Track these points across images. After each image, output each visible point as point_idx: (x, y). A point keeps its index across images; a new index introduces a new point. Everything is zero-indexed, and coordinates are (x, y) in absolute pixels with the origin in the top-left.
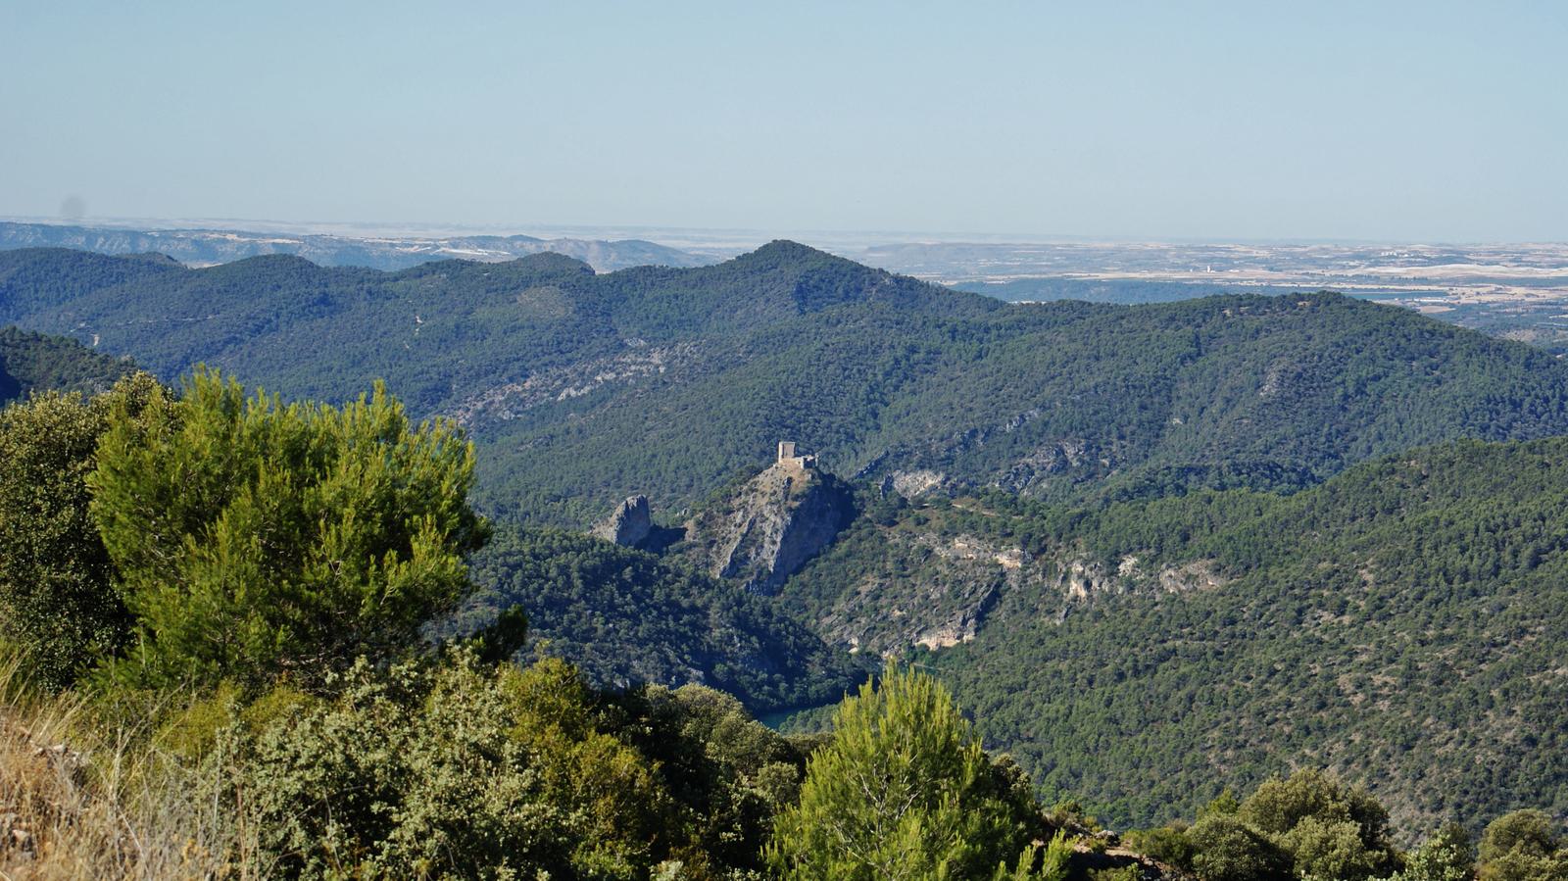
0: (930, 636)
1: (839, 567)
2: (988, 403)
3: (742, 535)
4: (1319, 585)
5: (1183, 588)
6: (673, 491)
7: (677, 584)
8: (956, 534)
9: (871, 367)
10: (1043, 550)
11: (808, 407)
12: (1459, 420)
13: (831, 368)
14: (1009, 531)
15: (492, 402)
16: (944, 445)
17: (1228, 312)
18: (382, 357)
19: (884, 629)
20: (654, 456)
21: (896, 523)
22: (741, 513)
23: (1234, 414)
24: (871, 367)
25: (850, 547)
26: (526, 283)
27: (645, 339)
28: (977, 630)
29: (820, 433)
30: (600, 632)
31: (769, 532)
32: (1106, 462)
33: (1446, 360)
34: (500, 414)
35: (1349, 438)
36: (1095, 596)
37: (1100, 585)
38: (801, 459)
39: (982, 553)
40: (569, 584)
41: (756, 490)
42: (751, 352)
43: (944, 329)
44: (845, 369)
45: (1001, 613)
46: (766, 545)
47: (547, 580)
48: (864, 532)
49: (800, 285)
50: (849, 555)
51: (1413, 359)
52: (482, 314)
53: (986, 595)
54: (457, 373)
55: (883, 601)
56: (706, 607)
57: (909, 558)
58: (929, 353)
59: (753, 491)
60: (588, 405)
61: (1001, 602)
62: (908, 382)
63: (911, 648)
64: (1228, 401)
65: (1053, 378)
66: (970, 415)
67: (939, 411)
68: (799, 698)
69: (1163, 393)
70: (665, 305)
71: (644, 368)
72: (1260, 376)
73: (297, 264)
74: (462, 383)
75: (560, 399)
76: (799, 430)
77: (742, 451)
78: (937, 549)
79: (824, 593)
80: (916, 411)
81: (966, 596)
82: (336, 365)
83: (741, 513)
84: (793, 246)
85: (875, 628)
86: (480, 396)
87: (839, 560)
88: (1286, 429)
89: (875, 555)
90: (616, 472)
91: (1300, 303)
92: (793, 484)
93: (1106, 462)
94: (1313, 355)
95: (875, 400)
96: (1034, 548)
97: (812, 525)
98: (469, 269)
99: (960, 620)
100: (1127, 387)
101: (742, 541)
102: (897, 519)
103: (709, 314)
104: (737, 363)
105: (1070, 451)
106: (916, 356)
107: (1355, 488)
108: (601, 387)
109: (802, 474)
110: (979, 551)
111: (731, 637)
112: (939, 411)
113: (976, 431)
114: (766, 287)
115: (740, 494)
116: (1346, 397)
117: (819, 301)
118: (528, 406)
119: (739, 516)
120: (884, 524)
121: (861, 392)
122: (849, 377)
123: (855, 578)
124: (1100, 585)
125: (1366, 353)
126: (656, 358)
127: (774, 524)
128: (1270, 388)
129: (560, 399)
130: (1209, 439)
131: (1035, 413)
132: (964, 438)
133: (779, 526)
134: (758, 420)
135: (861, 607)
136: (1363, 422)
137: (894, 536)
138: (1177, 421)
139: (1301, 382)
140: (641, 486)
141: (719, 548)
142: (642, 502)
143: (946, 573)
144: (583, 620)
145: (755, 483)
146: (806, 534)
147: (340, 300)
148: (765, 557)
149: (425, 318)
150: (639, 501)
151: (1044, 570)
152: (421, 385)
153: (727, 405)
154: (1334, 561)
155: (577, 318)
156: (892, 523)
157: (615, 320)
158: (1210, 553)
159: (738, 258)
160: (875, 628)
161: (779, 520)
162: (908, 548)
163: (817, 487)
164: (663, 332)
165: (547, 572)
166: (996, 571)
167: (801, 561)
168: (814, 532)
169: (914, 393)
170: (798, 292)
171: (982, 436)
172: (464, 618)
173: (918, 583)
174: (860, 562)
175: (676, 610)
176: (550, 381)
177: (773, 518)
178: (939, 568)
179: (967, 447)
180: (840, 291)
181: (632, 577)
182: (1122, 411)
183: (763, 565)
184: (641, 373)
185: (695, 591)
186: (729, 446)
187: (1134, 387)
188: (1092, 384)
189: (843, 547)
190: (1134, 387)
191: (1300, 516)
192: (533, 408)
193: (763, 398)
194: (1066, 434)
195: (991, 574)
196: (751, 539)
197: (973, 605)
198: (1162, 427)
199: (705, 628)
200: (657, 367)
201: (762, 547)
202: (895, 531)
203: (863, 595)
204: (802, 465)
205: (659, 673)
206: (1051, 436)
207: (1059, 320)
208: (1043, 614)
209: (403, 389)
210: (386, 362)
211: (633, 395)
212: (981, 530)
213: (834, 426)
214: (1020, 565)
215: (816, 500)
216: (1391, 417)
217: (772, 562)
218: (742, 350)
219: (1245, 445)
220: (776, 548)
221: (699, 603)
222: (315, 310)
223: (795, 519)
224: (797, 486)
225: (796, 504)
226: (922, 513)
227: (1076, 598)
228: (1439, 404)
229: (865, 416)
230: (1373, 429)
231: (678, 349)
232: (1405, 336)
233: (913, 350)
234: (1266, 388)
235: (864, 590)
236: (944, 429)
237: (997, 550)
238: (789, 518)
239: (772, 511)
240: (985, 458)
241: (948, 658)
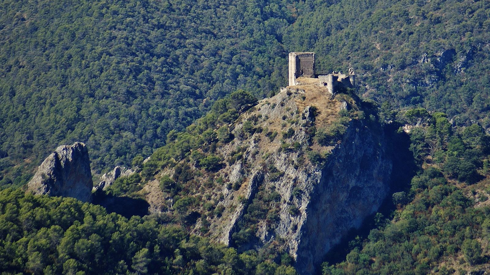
2: (465, 8)
3: (243, 201)
11: (180, 24)
22: (237, 167)
25: (414, 215)
29: (206, 64)
38: (329, 79)
41: (260, 130)
46: (283, 216)
48: (433, 193)
50: (414, 228)
67: (387, 26)
76: (176, 59)
77: (98, 93)
83: (237, 167)
87: (397, 237)
92: (319, 118)
95: (272, 14)
97: (352, 183)
101: (245, 211)
102: (482, 172)
109: (331, 102)
112: (387, 26)
115: (232, 137)
120: (462, 180)
127: (293, 179)
132: (435, 63)
133: (303, 186)
141: (207, 224)
142: (81, 155)
146: (343, 196)
148: (283, 236)
150: (75, 151)
161: (302, 177)
163: (355, 123)
165: (26, 260)
167: (337, 241)
168: (355, 194)
171: (463, 59)
174: (433, 239)
177: (291, 173)
179: (441, 77)
181: (148, 266)
183: (281, 248)
193: (115, 13)
201: (277, 220)
204: (330, 88)
215: (356, 142)
217: (295, 244)
220: (300, 222)
223: (327, 173)
224: (325, 121)
225: (327, 150)
229: (264, 38)
236: (402, 50)
238: (319, 173)
239: (289, 162)
240: (472, 91)
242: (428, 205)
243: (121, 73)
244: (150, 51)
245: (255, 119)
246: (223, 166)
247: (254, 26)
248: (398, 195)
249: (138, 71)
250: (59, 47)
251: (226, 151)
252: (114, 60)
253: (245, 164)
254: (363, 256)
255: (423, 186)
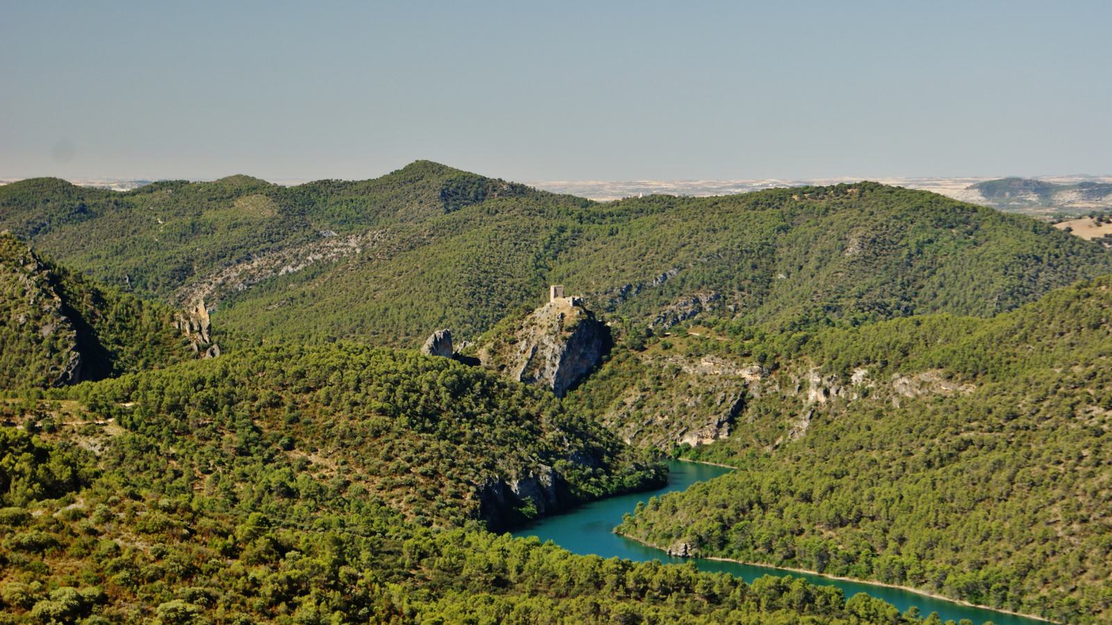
0: (691, 436)
1: (605, 383)
4: (1083, 385)
5: (919, 392)
6: (407, 335)
7: (514, 396)
8: (700, 355)
9: (533, 242)
10: (777, 366)
11: (495, 271)
12: (1001, 271)
13: (506, 243)
14: (746, 351)
15: (228, 278)
16: (608, 297)
17: (795, 197)
18: (138, 247)
19: (651, 432)
20: (386, 309)
21: (646, 349)
22: (525, 342)
23: (831, 268)
24: (533, 242)
26: (238, 193)
27: (336, 231)
28: (730, 431)
30: (468, 436)
31: (549, 356)
32: (732, 307)
33: (977, 228)
34: (236, 286)
35: (917, 286)
36: (833, 401)
37: (837, 392)
38: (570, 299)
39: (726, 370)
40: (438, 399)
42: (432, 235)
43: (574, 216)
44: (515, 244)
45: (748, 416)
46: (547, 367)
47: (422, 394)
48: (622, 356)
49: (443, 191)
50: (613, 373)
51: (952, 227)
52: (209, 215)
53: (735, 403)
54: (197, 258)
55: (646, 410)
56: (538, 415)
57: (663, 375)
58: (573, 232)
59: (532, 325)
60: (304, 278)
61: (747, 408)
62: (563, 253)
63: (676, 446)
64: (821, 260)
65: (684, 246)
66: (623, 274)
67: (598, 273)
68: (618, 487)
69: (769, 255)
70: (344, 207)
71: (344, 250)
72: (843, 242)
73: (60, 184)
74: (201, 265)
75: (281, 274)
78: (685, 368)
79: (595, 405)
80: (574, 274)
81: (718, 403)
82: (103, 254)
83: (525, 342)
84: (433, 164)
85: (642, 431)
86: (219, 273)
87: (604, 378)
88: (870, 280)
89: (632, 374)
90: (359, 322)
91: (849, 191)
93: (732, 307)
94: (882, 225)
95: (541, 266)
96: (768, 365)
97: (582, 351)
98: (187, 186)
99: (716, 423)
100: (741, 251)
101: (528, 364)
102: (646, 346)
103: (377, 213)
104: (423, 243)
105: (704, 300)
106: (565, 234)
107: (1058, 309)
108: (312, 265)
109: (572, 311)
110: (723, 369)
111: (561, 438)
112: (598, 273)
113: (631, 286)
114: (419, 192)
116: (910, 256)
117: (458, 202)
118: (257, 280)
119: (523, 345)
121: (530, 261)
122: (519, 249)
123: (619, 392)
124: (837, 392)
125: (918, 223)
126: (353, 243)
127: (552, 349)
128: (853, 249)
129: (281, 274)
130: (814, 289)
131: (674, 272)
134: (463, 281)
135: (629, 415)
136: (926, 273)
137: (646, 358)
138: (781, 276)
139: (876, 246)
140: (381, 331)
141: (509, 370)
142: (447, 335)
143: (697, 385)
144: (454, 426)
145: (534, 318)
146: (577, 357)
147: (94, 210)
149: (164, 219)
150: (444, 334)
151: (780, 382)
152: (171, 267)
153: (436, 271)
154: (1087, 365)
155: (281, 217)
156: (642, 349)
157: (309, 218)
158: (939, 364)
159: (392, 173)
160: (642, 431)
161: (557, 347)
162: (661, 367)
163: (583, 321)
164: (346, 224)
166: (741, 384)
168: (583, 356)
169: (569, 260)
170: (442, 195)
172: (363, 426)
173: (674, 394)
175: (514, 418)
176: (272, 261)
177: (551, 345)
178: (691, 383)
179: (625, 298)
180: (472, 195)
181: (481, 391)
182: (739, 269)
184: (342, 254)
185: (528, 401)
186: (444, 301)
187: (747, 252)
188: (715, 249)
189: (606, 369)
190: (747, 252)
191: (1012, 333)
192: (261, 282)
194: (699, 288)
195: (737, 386)
196: (534, 362)
197: (725, 411)
198: (770, 281)
199: (539, 432)
200: (354, 249)
201: (544, 369)
202: (645, 354)
203: (629, 405)
204: (571, 303)
205: (520, 469)
206: (689, 289)
207: (655, 209)
208: (787, 417)
209: (157, 270)
210: (142, 251)
211: (346, 268)
212: (723, 351)
213: (516, 285)
214: (759, 378)
215: (584, 330)
216: (948, 269)
218: (427, 233)
219: (843, 292)
220: (556, 370)
221: (533, 411)
222: (77, 216)
223: (569, 346)
225: (570, 334)
226: (668, 340)
227: (817, 404)
228: (983, 259)
230: (935, 279)
231: (369, 235)
232: (943, 211)
233: (562, 230)
234: (850, 250)
235: (629, 401)
236: (606, 284)
237: (739, 366)
240: (640, 306)
241: (710, 454)
242: (619, 362)
243: (466, 295)
244: (480, 284)
245: (534, 318)
246: (517, 342)
247: (532, 272)
248: (605, 357)
249: (474, 294)
250: (435, 281)
251: (519, 334)
252: (463, 288)
253: (528, 340)
254: (587, 387)
255: (617, 353)
